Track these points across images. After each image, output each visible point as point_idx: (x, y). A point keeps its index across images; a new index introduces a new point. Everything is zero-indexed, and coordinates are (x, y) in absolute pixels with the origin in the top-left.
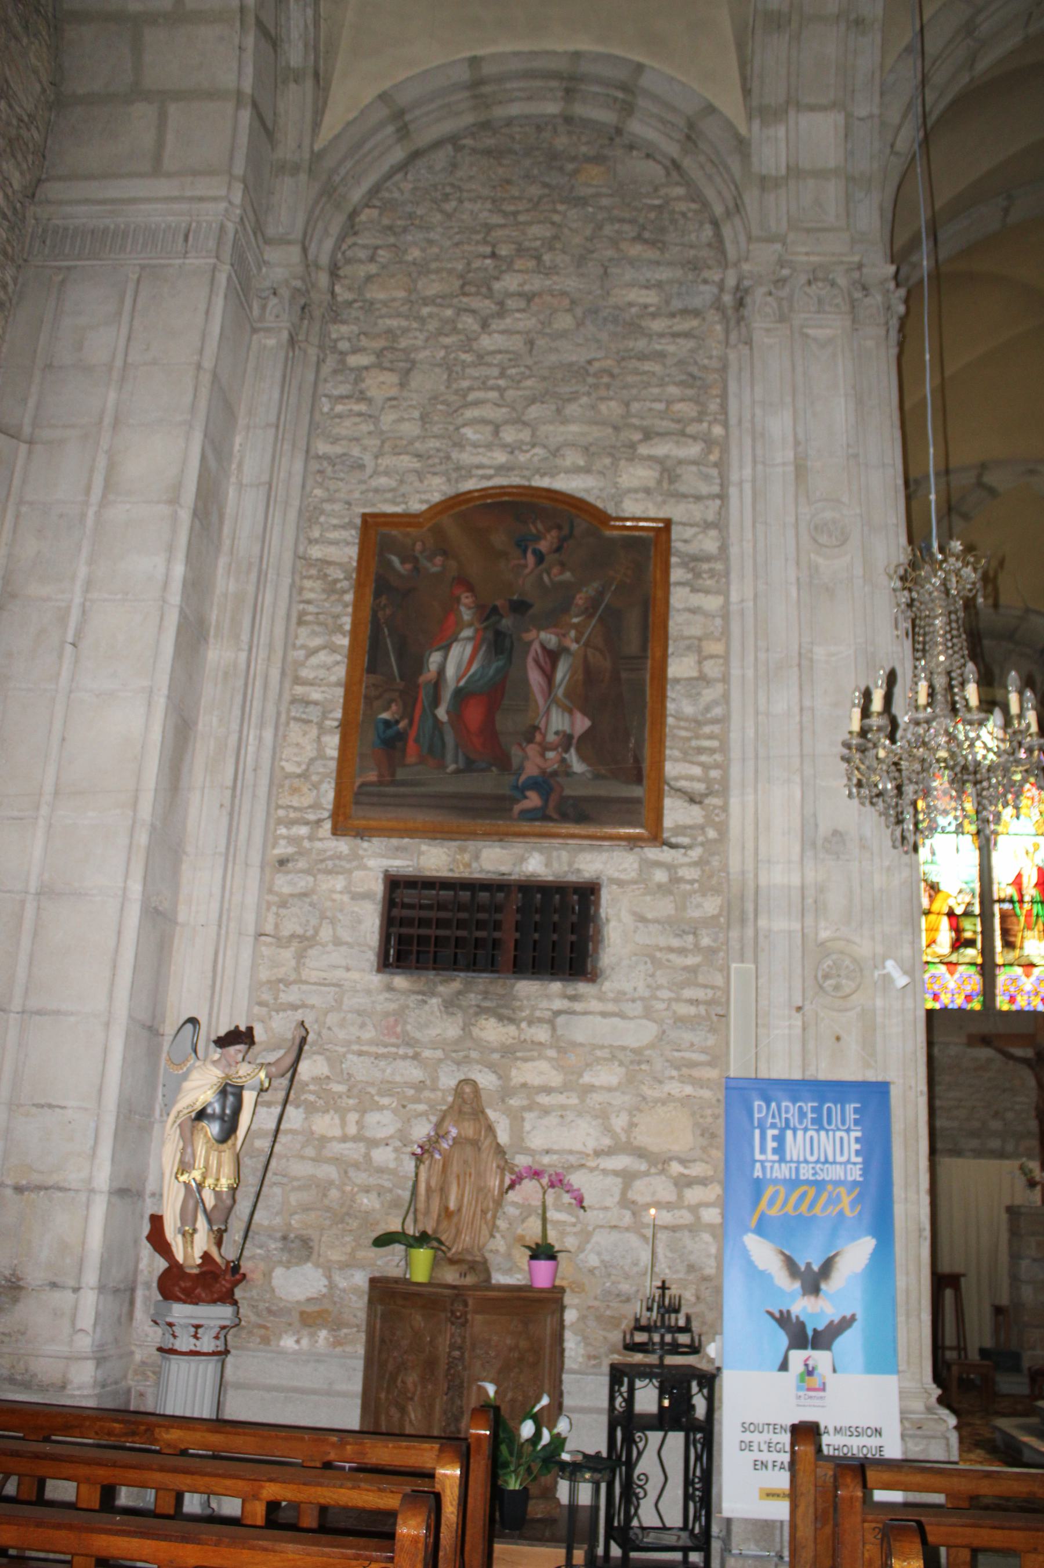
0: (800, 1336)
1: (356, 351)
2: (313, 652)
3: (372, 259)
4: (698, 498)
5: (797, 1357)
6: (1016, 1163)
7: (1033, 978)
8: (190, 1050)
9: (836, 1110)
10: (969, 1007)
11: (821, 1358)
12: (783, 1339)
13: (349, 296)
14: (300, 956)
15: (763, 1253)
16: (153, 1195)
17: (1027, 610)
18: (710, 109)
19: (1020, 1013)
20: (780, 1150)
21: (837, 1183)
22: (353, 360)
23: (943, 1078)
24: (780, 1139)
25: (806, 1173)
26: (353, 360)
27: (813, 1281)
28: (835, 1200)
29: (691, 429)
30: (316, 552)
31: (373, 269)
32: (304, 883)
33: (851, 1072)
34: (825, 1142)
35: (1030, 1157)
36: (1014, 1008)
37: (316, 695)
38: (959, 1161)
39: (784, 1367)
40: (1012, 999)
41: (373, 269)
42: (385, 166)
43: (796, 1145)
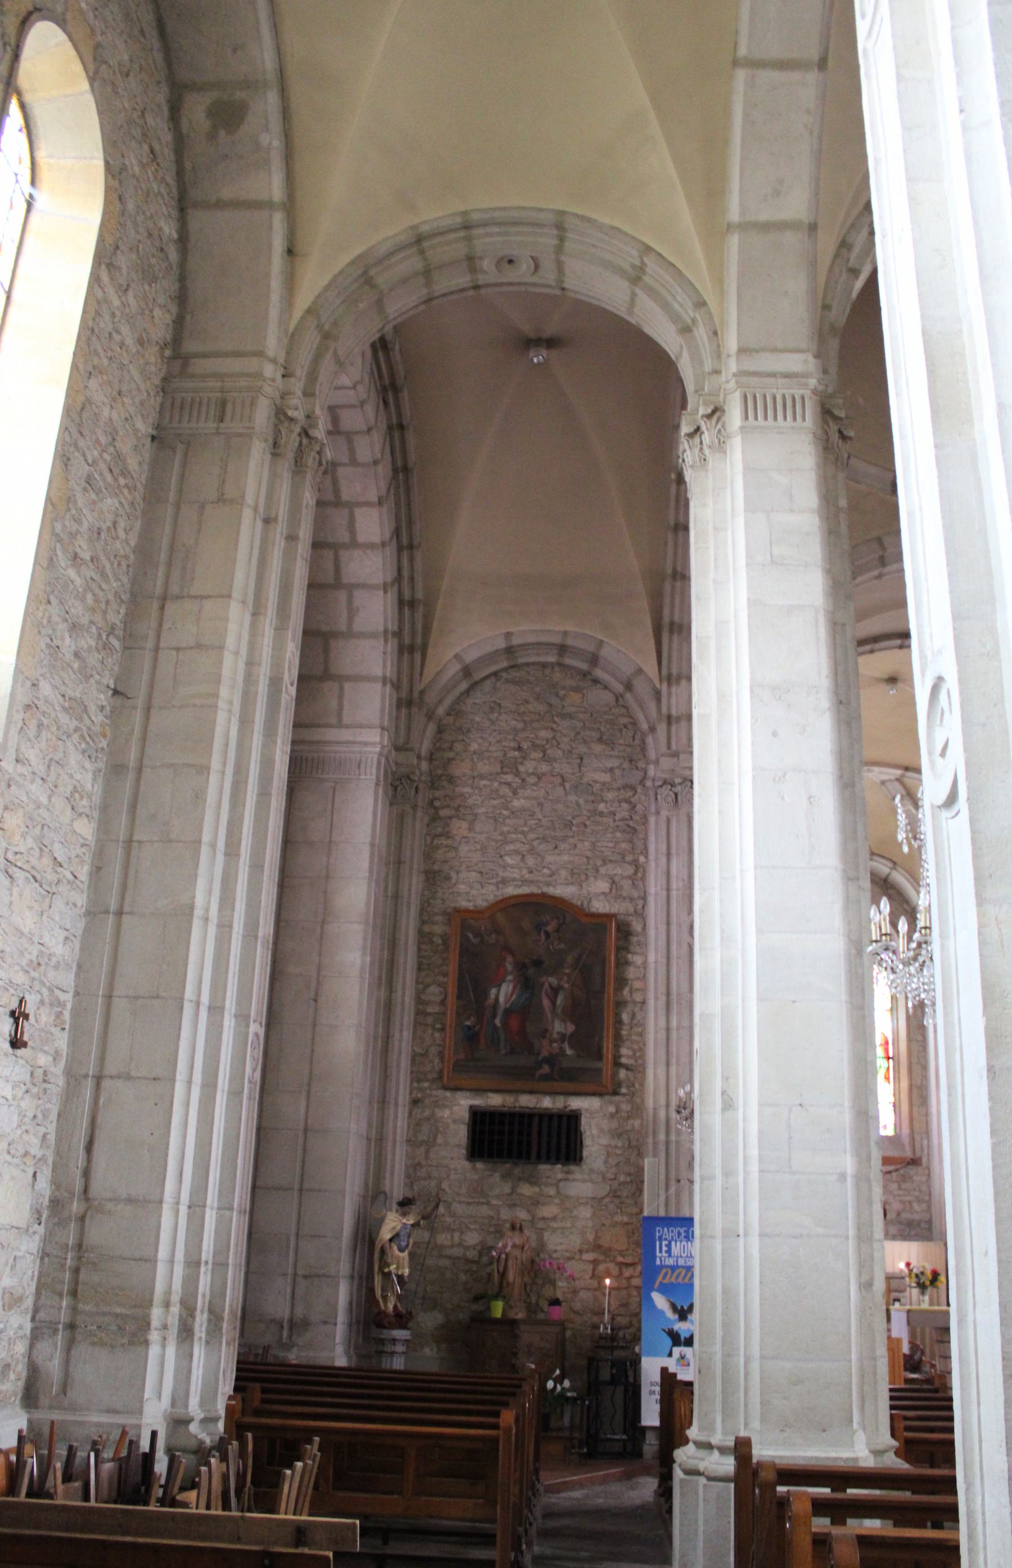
0: (676, 1339)
5: (676, 1351)
12: (668, 1341)
14: (427, 1152)
15: (660, 1301)
18: (640, 671)
20: (669, 1251)
24: (669, 1246)
25: (681, 1262)
32: (427, 1113)
37: (430, 1010)
39: (670, 1355)
43: (676, 1249)
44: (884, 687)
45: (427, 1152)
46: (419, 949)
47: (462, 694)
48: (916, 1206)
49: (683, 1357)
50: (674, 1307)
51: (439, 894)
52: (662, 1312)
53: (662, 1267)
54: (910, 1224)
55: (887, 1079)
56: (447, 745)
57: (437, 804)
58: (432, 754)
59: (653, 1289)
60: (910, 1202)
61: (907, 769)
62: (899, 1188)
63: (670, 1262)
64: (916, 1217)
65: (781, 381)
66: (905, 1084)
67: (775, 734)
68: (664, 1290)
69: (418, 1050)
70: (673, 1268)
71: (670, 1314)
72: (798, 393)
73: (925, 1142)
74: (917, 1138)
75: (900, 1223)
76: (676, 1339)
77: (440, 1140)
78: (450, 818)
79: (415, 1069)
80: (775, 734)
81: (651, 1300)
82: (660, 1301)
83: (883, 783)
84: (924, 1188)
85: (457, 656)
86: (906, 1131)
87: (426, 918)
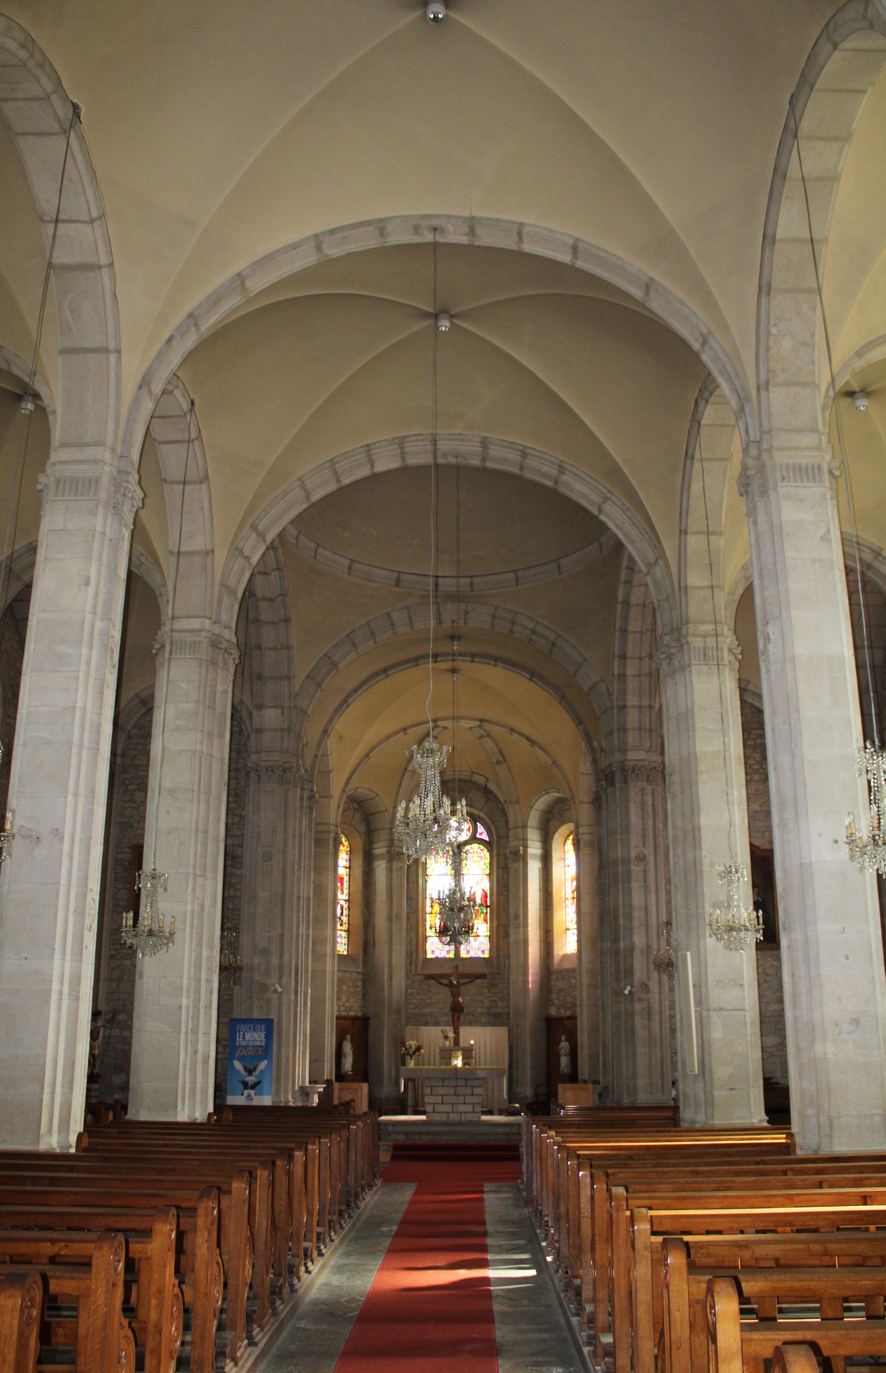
0: (246, 1085)
1: (132, 784)
2: (120, 890)
3: (135, 749)
4: (237, 837)
5: (246, 1092)
6: (439, 1029)
7: (478, 942)
8: (196, 404)
9: (259, 1026)
10: (448, 956)
11: (252, 1092)
12: (242, 1087)
13: (129, 763)
14: (118, 985)
15: (238, 1065)
16: (382, 232)
17: (473, 772)
19: (472, 958)
20: (244, 1038)
21: (258, 1046)
22: (131, 787)
23: (220, 1026)
24: (244, 1035)
25: (251, 1043)
26: (131, 787)
27: (250, 1072)
28: (257, 1051)
29: (236, 812)
30: (120, 856)
31: (136, 752)
32: (118, 963)
33: (263, 1017)
34: (256, 1035)
35: (447, 1024)
36: (468, 956)
37: (120, 904)
38: (427, 1028)
39: (242, 1094)
40: (468, 952)
41: (136, 752)
42: (139, 715)
44: (449, 675)
45: (118, 985)
46: (115, 869)
47: (142, 715)
48: (500, 1003)
49: (249, 1095)
50: (245, 1068)
51: (636, 597)
52: (239, 1071)
53: (240, 1046)
54: (496, 1015)
55: (486, 920)
56: (133, 747)
57: (127, 782)
58: (124, 752)
59: (234, 1059)
60: (496, 1001)
61: (482, 721)
62: (489, 992)
63: (244, 1043)
64: (500, 1011)
65: (188, 634)
66: (495, 924)
67: (168, 812)
68: (241, 1059)
69: (114, 927)
70: (246, 1047)
71: (243, 1072)
72: (197, 639)
73: (507, 961)
74: (502, 958)
75: (489, 1014)
76: (246, 1085)
77: (125, 978)
78: (134, 790)
79: (749, 778)
80: (168, 812)
81: (233, 1064)
82: (238, 1065)
83: (471, 728)
84: (505, 992)
85: (137, 695)
86: (495, 955)
87: (119, 850)
